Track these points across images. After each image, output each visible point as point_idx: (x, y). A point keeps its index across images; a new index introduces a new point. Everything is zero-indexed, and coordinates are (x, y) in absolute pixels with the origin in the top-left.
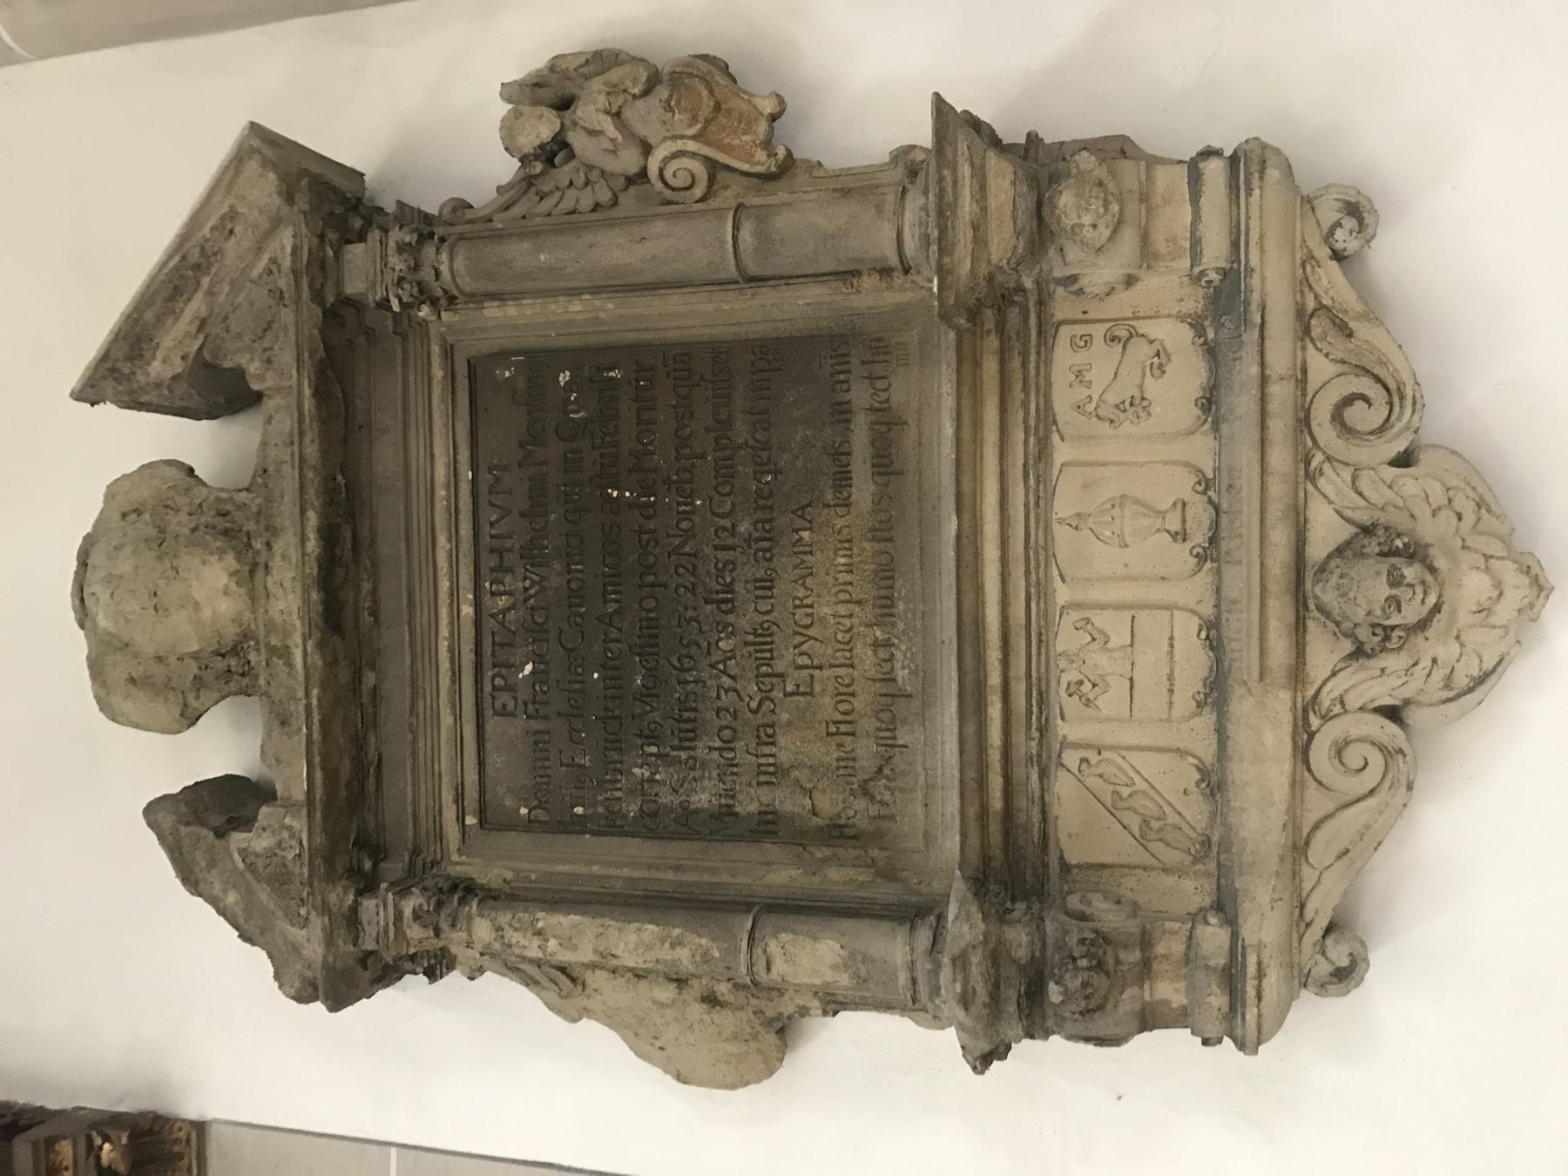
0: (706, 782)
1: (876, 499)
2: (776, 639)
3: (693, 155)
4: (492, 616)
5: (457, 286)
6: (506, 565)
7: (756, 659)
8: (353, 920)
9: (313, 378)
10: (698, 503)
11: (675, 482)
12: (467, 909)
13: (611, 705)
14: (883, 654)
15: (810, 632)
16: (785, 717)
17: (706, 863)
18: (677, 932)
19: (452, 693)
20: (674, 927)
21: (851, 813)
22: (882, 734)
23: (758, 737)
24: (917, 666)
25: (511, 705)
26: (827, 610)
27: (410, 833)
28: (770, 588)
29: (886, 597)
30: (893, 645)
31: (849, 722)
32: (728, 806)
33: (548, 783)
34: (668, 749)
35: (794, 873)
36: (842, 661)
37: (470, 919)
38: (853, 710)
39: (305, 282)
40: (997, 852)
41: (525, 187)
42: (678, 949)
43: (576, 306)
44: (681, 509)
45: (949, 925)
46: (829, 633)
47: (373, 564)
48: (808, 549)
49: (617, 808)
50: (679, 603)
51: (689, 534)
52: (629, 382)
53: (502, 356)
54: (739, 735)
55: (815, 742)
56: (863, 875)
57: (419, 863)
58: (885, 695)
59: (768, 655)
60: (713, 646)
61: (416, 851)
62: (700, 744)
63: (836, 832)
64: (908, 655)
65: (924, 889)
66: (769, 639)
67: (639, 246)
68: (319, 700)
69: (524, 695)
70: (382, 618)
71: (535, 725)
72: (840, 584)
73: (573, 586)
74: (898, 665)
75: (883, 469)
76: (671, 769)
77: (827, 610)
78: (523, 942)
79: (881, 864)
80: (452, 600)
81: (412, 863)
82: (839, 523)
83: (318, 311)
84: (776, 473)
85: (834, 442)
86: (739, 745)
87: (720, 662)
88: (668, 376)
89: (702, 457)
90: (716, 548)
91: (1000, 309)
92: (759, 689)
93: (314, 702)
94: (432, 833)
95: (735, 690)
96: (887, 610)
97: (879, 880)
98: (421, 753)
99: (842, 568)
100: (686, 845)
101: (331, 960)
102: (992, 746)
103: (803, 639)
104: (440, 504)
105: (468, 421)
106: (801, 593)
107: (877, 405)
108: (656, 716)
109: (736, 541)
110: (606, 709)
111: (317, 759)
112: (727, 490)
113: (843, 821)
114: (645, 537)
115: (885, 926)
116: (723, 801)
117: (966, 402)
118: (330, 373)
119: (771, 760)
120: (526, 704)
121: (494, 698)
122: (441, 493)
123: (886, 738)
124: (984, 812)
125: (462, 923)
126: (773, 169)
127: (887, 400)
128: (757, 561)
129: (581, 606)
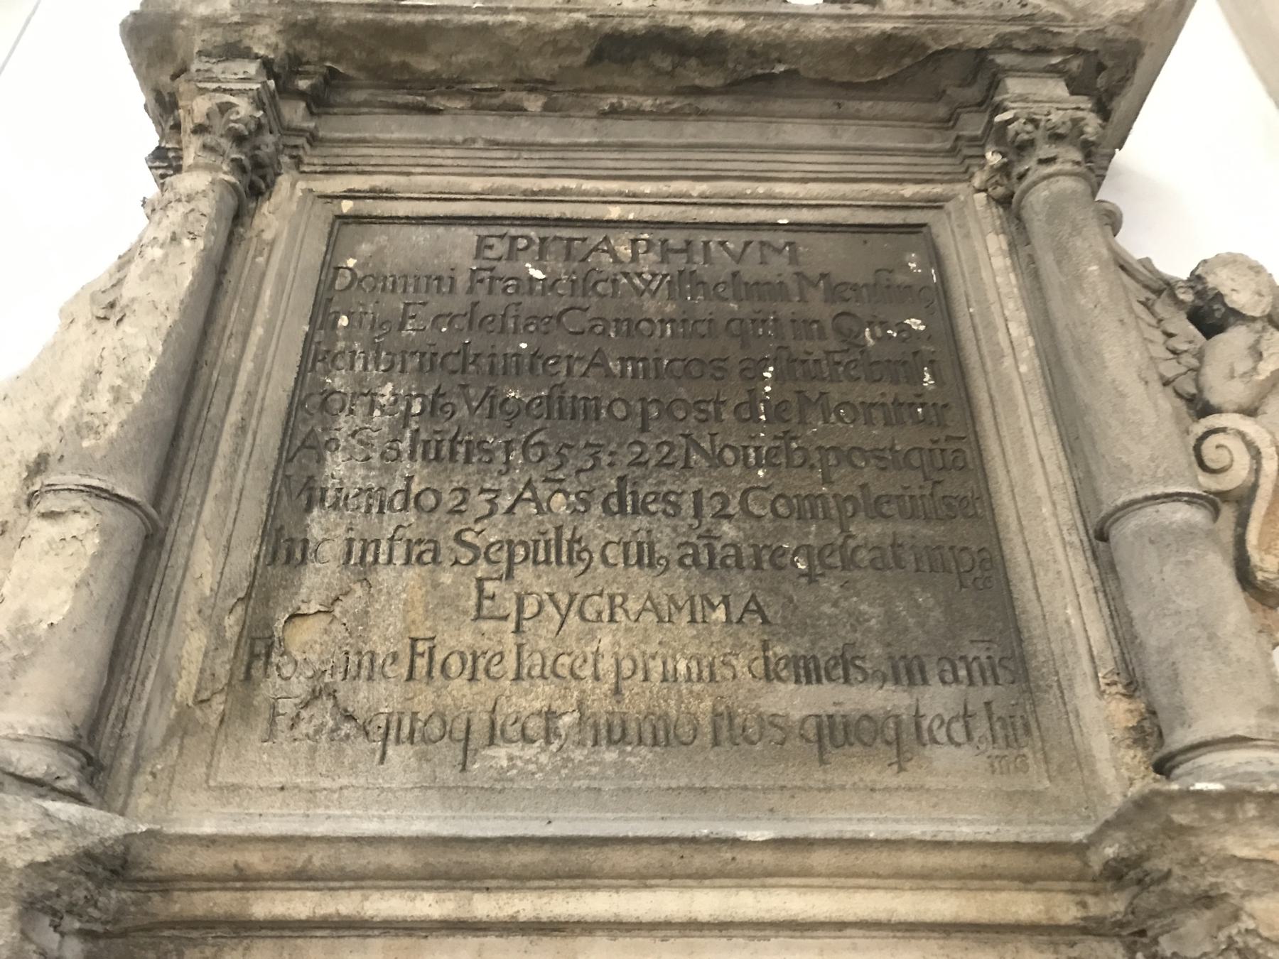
0: (362, 472)
1: (778, 721)
2: (565, 569)
3: (1257, 471)
4: (606, 239)
5: (1035, 183)
6: (671, 256)
7: (536, 542)
8: (234, 51)
9: (905, 33)
10: (761, 473)
11: (788, 446)
12: (225, 168)
13: (483, 361)
14: (535, 725)
15: (573, 619)
16: (446, 578)
17: (243, 465)
18: (137, 397)
19: (510, 190)
20: (145, 396)
21: (287, 671)
22: (406, 723)
23: (420, 542)
24: (512, 780)
25: (489, 253)
26: (606, 642)
27: (337, 135)
28: (639, 561)
29: (624, 731)
30: (548, 742)
31: (429, 672)
32: (323, 500)
33: (384, 289)
34: (414, 426)
35: (207, 584)
36: (527, 663)
37: (210, 168)
38: (447, 677)
39: (1020, 28)
40: (160, 907)
41: (1156, 286)
42: (109, 396)
43: (1018, 330)
44: (751, 451)
45: (39, 801)
46: (571, 643)
47: (673, 112)
48: (699, 617)
49: (340, 363)
50: (620, 445)
51: (716, 460)
52: (919, 396)
53: (935, 258)
54: (425, 516)
55: (404, 620)
56: (185, 687)
57: (301, 141)
58: (468, 728)
59: (541, 557)
60: (557, 486)
61: (314, 139)
62: (417, 466)
63: (260, 648)
64: (532, 767)
65: (143, 779)
66: (564, 559)
67: (1135, 376)
68: (512, 24)
69: (503, 268)
70: (608, 122)
71: (462, 280)
72: (645, 665)
73: (644, 325)
74: (515, 750)
75: (826, 731)
76: (385, 429)
77: (606, 642)
78: (166, 222)
79: (198, 713)
80: (627, 196)
81: (299, 132)
82: (740, 664)
83: (986, 42)
84: (810, 576)
85: (863, 658)
86: (411, 516)
87: (534, 493)
88: (935, 442)
89: (826, 480)
90: (698, 493)
91: (1121, 925)
92: (492, 544)
93: (510, 18)
94: (335, 161)
95: (491, 513)
96: (604, 732)
97: (174, 710)
98: (438, 152)
99: (670, 667)
100: (275, 442)
101: (184, 22)
102: (366, 898)
103: (563, 607)
104: (747, 187)
105: (850, 222)
106: (633, 606)
107: (925, 724)
108: (463, 412)
109: (708, 519)
110: (477, 356)
111: (439, 17)
112: (782, 510)
113: (275, 658)
114: (711, 408)
115: (80, 705)
116: (331, 493)
117: (964, 860)
118: (907, 61)
119: (383, 558)
120: (492, 269)
121: (502, 237)
122: (761, 188)
123: (399, 729)
124: (245, 880)
125: (208, 158)
126: (1260, 576)
127: (934, 741)
128: (681, 545)
129: (617, 333)
